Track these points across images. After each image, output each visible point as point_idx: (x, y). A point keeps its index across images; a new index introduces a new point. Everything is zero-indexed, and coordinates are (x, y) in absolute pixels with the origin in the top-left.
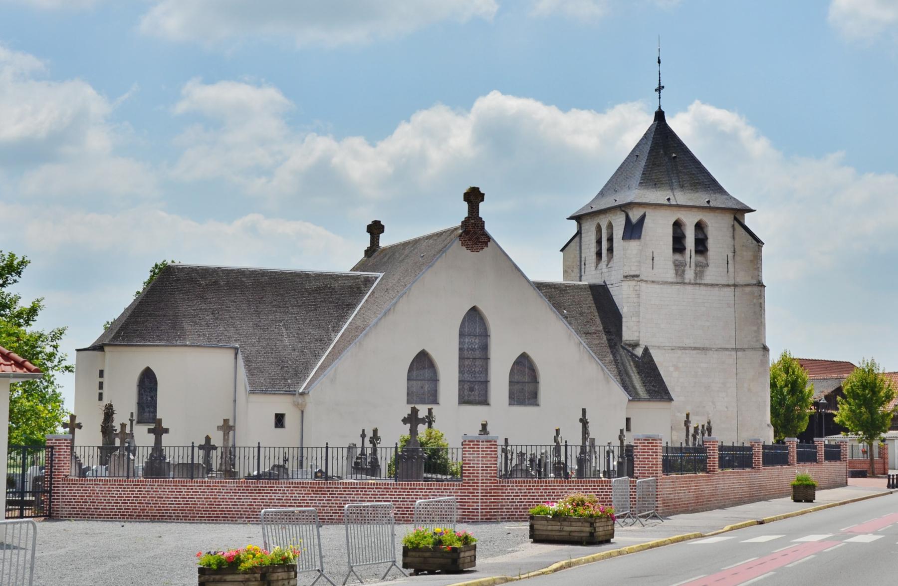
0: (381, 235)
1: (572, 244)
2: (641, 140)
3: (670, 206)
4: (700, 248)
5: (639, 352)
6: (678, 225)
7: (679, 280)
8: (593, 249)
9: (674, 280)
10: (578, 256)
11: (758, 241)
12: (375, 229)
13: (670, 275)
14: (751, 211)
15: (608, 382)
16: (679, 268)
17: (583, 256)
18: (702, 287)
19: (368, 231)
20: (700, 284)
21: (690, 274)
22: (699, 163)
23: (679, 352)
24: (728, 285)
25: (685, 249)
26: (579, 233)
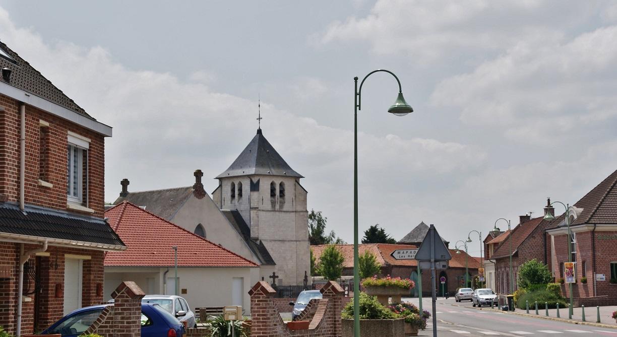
0: (128, 186)
1: (217, 191)
2: (251, 143)
3: (271, 175)
4: (282, 195)
5: (258, 242)
6: (272, 184)
7: (273, 209)
8: (229, 194)
9: (271, 209)
10: (220, 196)
11: (307, 192)
12: (125, 183)
13: (269, 207)
14: (302, 177)
15: (252, 257)
16: (273, 204)
17: (223, 196)
18: (283, 213)
19: (121, 184)
20: (282, 211)
21: (277, 207)
22: (278, 155)
23: (273, 242)
24: (293, 212)
25: (275, 195)
26: (220, 186)
